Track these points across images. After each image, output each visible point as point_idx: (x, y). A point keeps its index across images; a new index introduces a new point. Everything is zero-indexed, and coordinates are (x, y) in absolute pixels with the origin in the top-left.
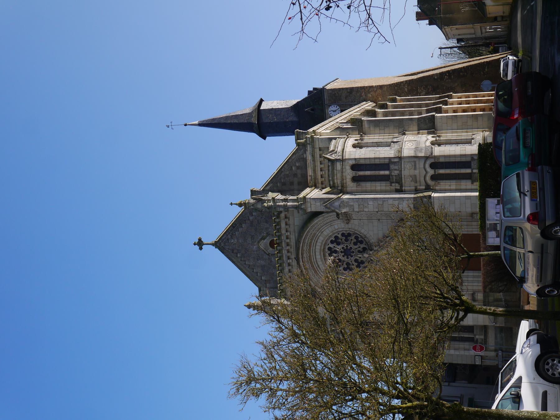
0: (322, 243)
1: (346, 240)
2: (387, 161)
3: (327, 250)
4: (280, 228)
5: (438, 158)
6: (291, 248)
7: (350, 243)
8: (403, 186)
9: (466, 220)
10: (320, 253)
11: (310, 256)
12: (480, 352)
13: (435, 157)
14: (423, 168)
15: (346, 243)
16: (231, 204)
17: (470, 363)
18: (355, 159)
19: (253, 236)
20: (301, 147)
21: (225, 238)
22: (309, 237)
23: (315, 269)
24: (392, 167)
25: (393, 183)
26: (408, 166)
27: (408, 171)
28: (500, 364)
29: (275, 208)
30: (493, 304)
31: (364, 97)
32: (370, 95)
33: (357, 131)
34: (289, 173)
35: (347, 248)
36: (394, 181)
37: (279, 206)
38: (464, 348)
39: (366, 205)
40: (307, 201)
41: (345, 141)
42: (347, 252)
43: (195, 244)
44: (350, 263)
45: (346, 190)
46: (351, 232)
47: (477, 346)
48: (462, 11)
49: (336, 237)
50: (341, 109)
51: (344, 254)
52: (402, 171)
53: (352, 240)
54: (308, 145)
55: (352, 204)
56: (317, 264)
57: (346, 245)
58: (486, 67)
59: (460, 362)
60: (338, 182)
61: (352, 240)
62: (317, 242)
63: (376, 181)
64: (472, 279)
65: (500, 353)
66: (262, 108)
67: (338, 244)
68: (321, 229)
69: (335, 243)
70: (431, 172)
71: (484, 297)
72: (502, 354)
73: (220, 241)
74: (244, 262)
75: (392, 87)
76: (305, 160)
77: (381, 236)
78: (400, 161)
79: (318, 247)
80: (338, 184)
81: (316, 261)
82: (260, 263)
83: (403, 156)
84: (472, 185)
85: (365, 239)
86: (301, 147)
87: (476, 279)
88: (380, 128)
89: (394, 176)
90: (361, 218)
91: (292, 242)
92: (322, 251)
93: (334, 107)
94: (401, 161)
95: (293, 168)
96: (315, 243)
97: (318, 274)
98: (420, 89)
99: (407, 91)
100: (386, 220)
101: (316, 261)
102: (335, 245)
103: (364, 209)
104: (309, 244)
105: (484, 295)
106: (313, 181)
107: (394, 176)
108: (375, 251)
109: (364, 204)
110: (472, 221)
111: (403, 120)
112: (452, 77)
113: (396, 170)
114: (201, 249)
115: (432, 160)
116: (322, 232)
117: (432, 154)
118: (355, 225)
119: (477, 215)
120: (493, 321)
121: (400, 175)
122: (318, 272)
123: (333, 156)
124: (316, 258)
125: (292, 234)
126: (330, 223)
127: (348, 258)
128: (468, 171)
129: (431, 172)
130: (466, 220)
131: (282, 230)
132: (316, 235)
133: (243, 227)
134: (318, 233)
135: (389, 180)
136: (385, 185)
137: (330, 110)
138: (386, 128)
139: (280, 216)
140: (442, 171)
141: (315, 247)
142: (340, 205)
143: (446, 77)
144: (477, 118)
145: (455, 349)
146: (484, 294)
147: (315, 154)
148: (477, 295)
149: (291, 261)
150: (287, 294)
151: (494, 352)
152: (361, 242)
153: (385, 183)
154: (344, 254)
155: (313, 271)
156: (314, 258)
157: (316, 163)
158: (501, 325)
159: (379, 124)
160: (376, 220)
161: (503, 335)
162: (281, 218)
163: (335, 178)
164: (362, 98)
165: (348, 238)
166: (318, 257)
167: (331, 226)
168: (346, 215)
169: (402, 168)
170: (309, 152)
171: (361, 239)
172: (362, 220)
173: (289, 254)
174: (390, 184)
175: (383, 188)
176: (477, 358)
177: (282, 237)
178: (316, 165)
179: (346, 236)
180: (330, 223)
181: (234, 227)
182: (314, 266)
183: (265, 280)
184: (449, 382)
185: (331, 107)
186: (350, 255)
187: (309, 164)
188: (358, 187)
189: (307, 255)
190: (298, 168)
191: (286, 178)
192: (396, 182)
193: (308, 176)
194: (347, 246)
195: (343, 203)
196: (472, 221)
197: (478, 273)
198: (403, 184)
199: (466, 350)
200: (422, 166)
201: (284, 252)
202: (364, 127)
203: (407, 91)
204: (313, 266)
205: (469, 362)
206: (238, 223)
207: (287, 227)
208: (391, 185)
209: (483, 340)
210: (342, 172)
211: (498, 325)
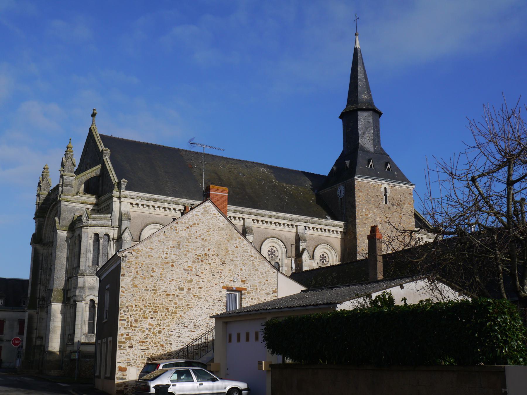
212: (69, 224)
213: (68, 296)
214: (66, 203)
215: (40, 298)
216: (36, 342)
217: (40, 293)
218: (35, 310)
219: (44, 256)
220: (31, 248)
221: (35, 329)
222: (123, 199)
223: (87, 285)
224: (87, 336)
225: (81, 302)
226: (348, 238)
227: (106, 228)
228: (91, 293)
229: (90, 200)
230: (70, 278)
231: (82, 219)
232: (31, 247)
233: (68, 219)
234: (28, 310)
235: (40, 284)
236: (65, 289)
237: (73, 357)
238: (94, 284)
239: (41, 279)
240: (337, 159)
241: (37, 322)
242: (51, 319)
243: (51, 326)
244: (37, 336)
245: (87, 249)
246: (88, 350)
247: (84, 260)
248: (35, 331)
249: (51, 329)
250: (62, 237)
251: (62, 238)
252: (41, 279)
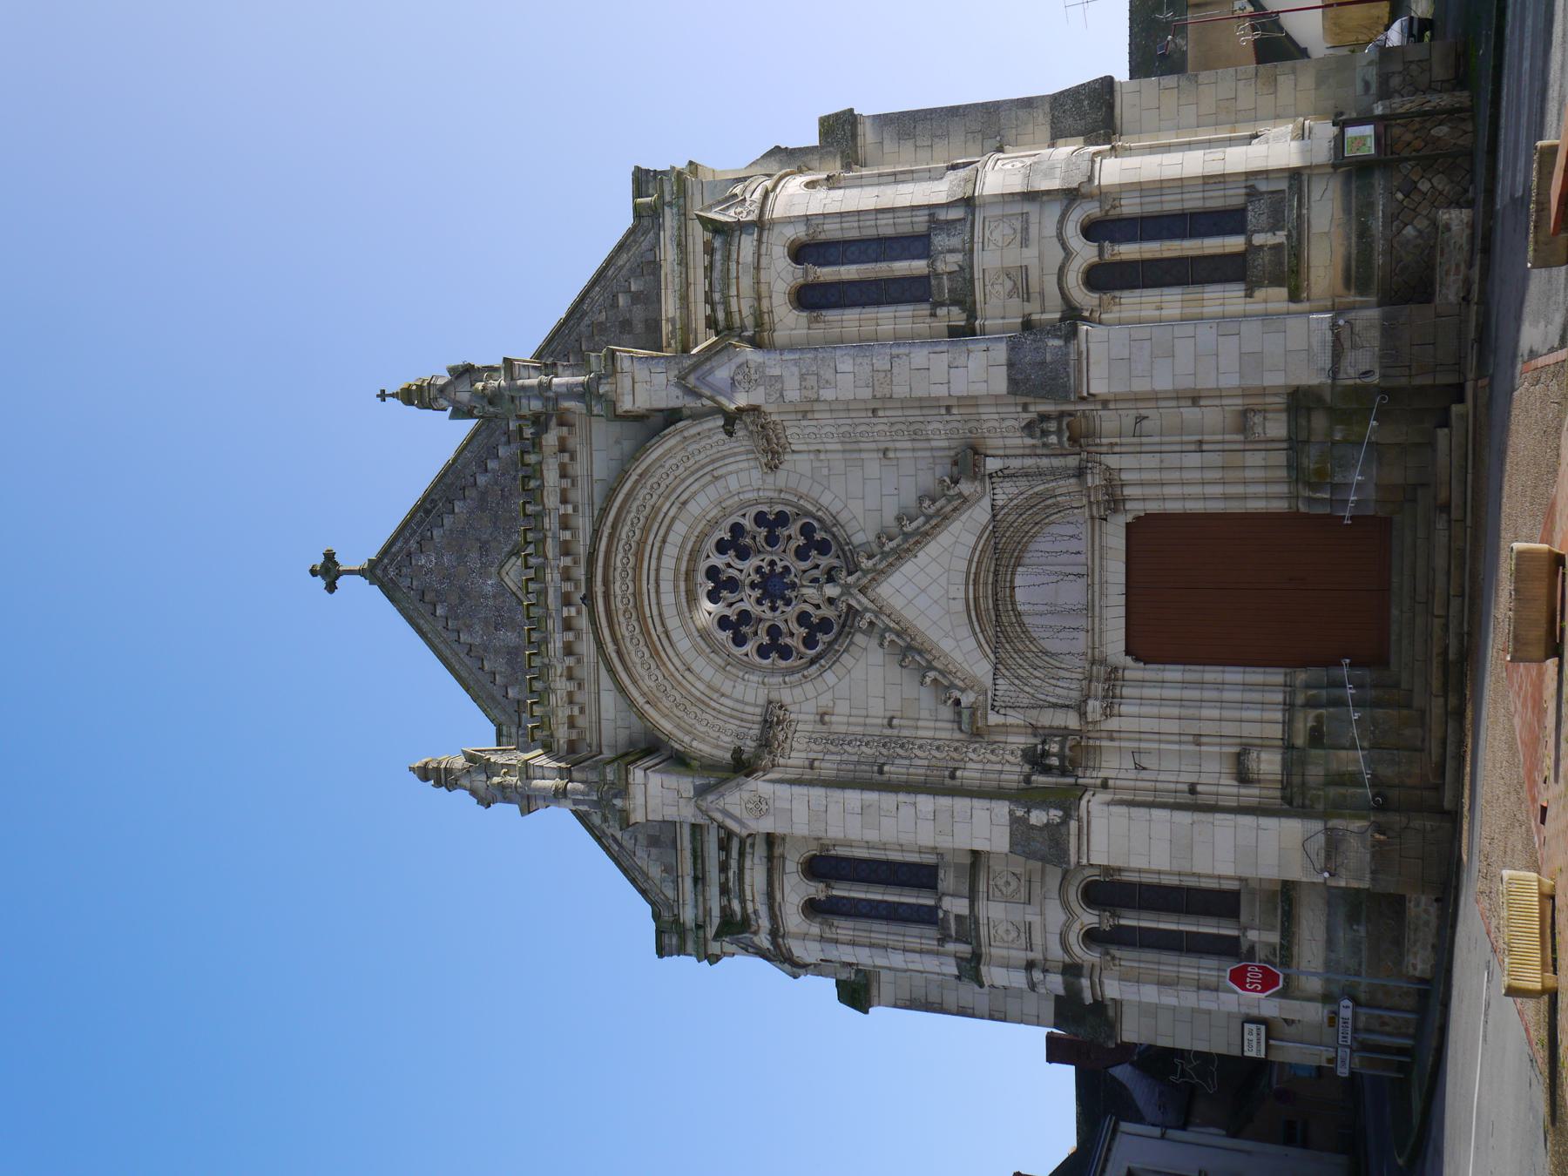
0: (682, 547)
1: (772, 540)
2: (920, 223)
3: (701, 577)
4: (541, 487)
5: (1114, 200)
6: (576, 562)
7: (784, 551)
8: (979, 313)
9: (1219, 447)
10: (676, 587)
11: (637, 594)
12: (1262, 991)
13: (1102, 195)
14: (1055, 240)
15: (768, 552)
16: (383, 396)
17: (1223, 1050)
18: (807, 219)
19: (487, 542)
20: (646, 224)
21: (401, 549)
22: (635, 521)
23: (653, 643)
24: (940, 241)
25: (942, 304)
26: (997, 235)
27: (999, 253)
28: (1343, 1062)
29: (513, 399)
30: (1321, 793)
33: (838, 157)
34: (607, 318)
35: (772, 570)
36: (946, 296)
37: (523, 388)
38: (1198, 980)
39: (828, 374)
40: (619, 370)
42: (773, 586)
43: (314, 572)
44: (782, 626)
45: (771, 339)
46: (787, 509)
47: (1249, 969)
48: (1243, 41)
49: (737, 529)
51: (760, 591)
53: (790, 537)
54: (667, 209)
55: (776, 372)
56: (663, 625)
57: (768, 558)
59: (1183, 1043)
60: (743, 307)
61: (790, 537)
62: (664, 541)
63: (883, 304)
64: (1237, 696)
65: (1346, 1010)
67: (743, 554)
68: (679, 491)
69: (732, 553)
70: (1086, 253)
71: (1287, 766)
72: (1355, 1016)
73: (386, 561)
74: (454, 636)
76: (652, 267)
77: (889, 518)
78: (970, 217)
79: (668, 562)
80: (742, 319)
81: (660, 615)
82: (504, 640)
83: (981, 196)
84: (1248, 300)
85: (834, 529)
86: (646, 222)
87: (1256, 696)
88: (918, 143)
89: (945, 277)
90: (821, 447)
91: (581, 543)
92: (682, 577)
94: (973, 215)
95: (622, 300)
96: (657, 545)
97: (664, 664)
100: (909, 454)
101: (660, 615)
102: (730, 558)
103: (821, 392)
104: (633, 544)
105: (1284, 760)
106: (679, 338)
107: (945, 277)
108: (865, 572)
109: (822, 372)
110: (1244, 450)
111: (998, 108)
113: (951, 251)
114: (331, 588)
115: (1092, 209)
116: (684, 503)
117: (1091, 179)
118: (801, 475)
119: (1265, 418)
120: (1320, 862)
121: (967, 270)
122: (663, 654)
123: (732, 212)
124: (658, 604)
125: (584, 514)
126: (711, 468)
127: (773, 609)
128: (1235, 243)
129: (1086, 253)
130: (1219, 447)
131: (545, 493)
132: (662, 515)
133: (456, 510)
134: (668, 505)
135: (928, 300)
136: (910, 313)
138: (936, 140)
139: (540, 443)
140: (1129, 251)
141: (659, 558)
142: (733, 379)
145: (1161, 983)
146: (1284, 753)
147: (690, 239)
148: (1258, 757)
149: (573, 611)
150: (555, 733)
151: (1319, 1005)
152: (824, 548)
153: (911, 307)
154: (763, 594)
155: (645, 650)
156: (653, 601)
157: (691, 272)
158: (1355, 884)
159: (915, 127)
160: (875, 455)
161: (1362, 931)
162: (544, 449)
163: (733, 292)
165: (778, 531)
166: (668, 599)
167: (717, 478)
168: (762, 427)
169: (976, 240)
170: (668, 233)
171: (824, 535)
172: (822, 456)
173: (568, 587)
174: (928, 312)
175: (905, 326)
176: (1251, 1033)
177: (546, 520)
178: (691, 280)
179: (772, 523)
180: (711, 468)
181: (428, 512)
182: (650, 634)
183: (518, 701)
184: (1165, 1127)
186: (783, 598)
187: (669, 277)
188: (812, 326)
189: (624, 587)
190: (636, 298)
191: (597, 338)
192: (954, 302)
193: (664, 322)
194: (772, 563)
195: (747, 370)
196: (1244, 450)
197: (1264, 673)
198: (978, 306)
199: (1207, 988)
200: (1051, 229)
201: (552, 577)
202: (860, 141)
204: (645, 632)
205: (1217, 1043)
206: (441, 499)
207: (566, 483)
208: (933, 315)
209: (1275, 949)
210: (758, 268)
211: (1343, 884)
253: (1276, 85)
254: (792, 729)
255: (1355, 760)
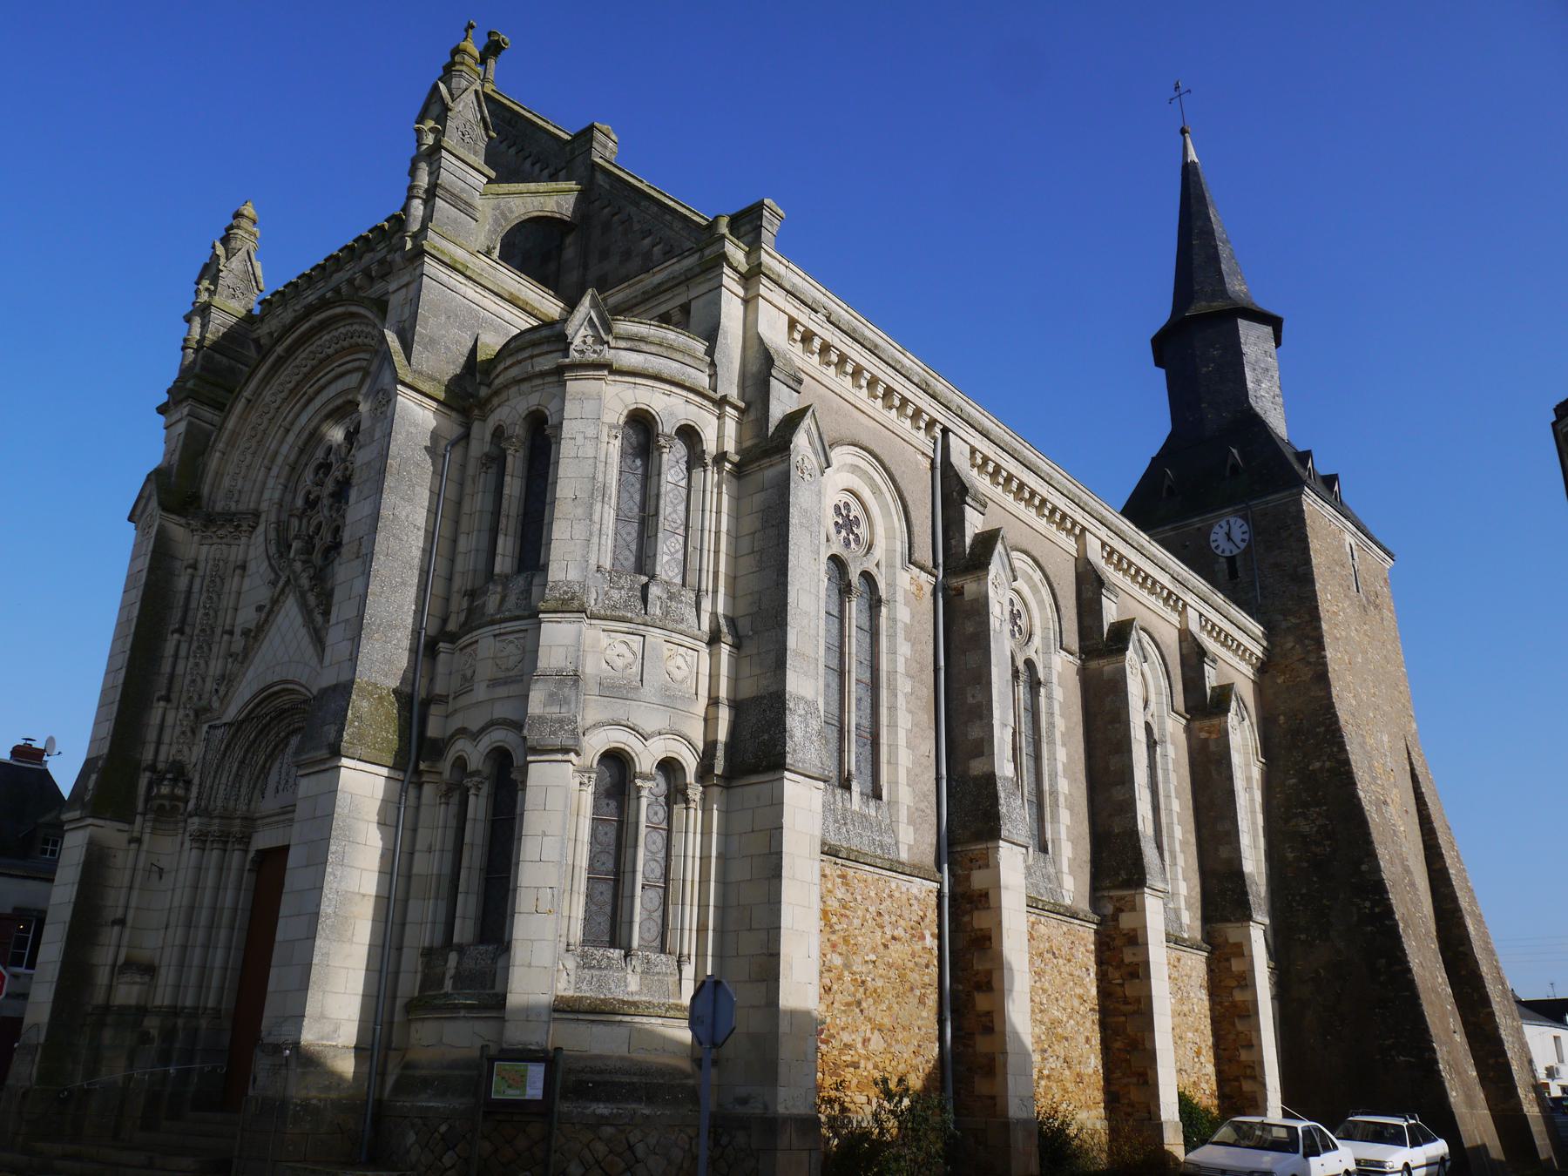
31: (1284, 625)
32: (1290, 645)
41: (665, 376)
50: (1238, 558)
52: (490, 628)
58: (1413, 1060)
66: (1243, 325)
75: (1324, 714)
93: (1243, 533)
98: (1319, 814)
99: (1311, 768)
105: (129, 1007)
112: (1369, 929)
137: (1232, 520)
138: (758, 557)
143: (1368, 904)
144: (764, 980)
148: (134, 983)
164: (1281, 617)
169: (503, 625)
185: (1240, 522)
203: (1311, 768)
212: (451, 374)
213: (433, 730)
214: (443, 273)
215: (161, 766)
216: (110, 987)
217: (159, 742)
218: (126, 827)
219: (200, 572)
220: (134, 533)
221: (114, 923)
222: (765, 288)
223: (592, 667)
224: (585, 964)
225: (559, 757)
226: (1280, 681)
227: (691, 396)
228: (620, 715)
229: (540, 301)
230: (474, 619)
231: (570, 331)
232: (127, 535)
233: (448, 348)
234: (90, 821)
235: (167, 699)
236: (411, 697)
237: (501, 1091)
238: (629, 666)
239: (172, 676)
240: (1154, 455)
241: (131, 888)
242: (333, 848)
243: (326, 891)
244: (121, 960)
245: (594, 478)
246: (596, 1049)
247: (579, 531)
248: (116, 929)
249: (326, 908)
250: (416, 425)
251: (412, 430)
252: (172, 676)
253: (758, 981)
254: (232, 542)
255: (114, 1071)
